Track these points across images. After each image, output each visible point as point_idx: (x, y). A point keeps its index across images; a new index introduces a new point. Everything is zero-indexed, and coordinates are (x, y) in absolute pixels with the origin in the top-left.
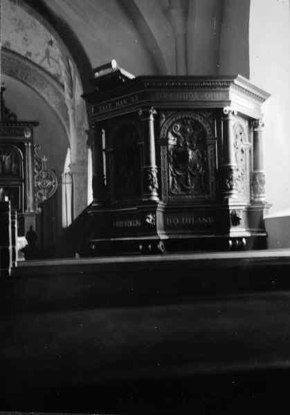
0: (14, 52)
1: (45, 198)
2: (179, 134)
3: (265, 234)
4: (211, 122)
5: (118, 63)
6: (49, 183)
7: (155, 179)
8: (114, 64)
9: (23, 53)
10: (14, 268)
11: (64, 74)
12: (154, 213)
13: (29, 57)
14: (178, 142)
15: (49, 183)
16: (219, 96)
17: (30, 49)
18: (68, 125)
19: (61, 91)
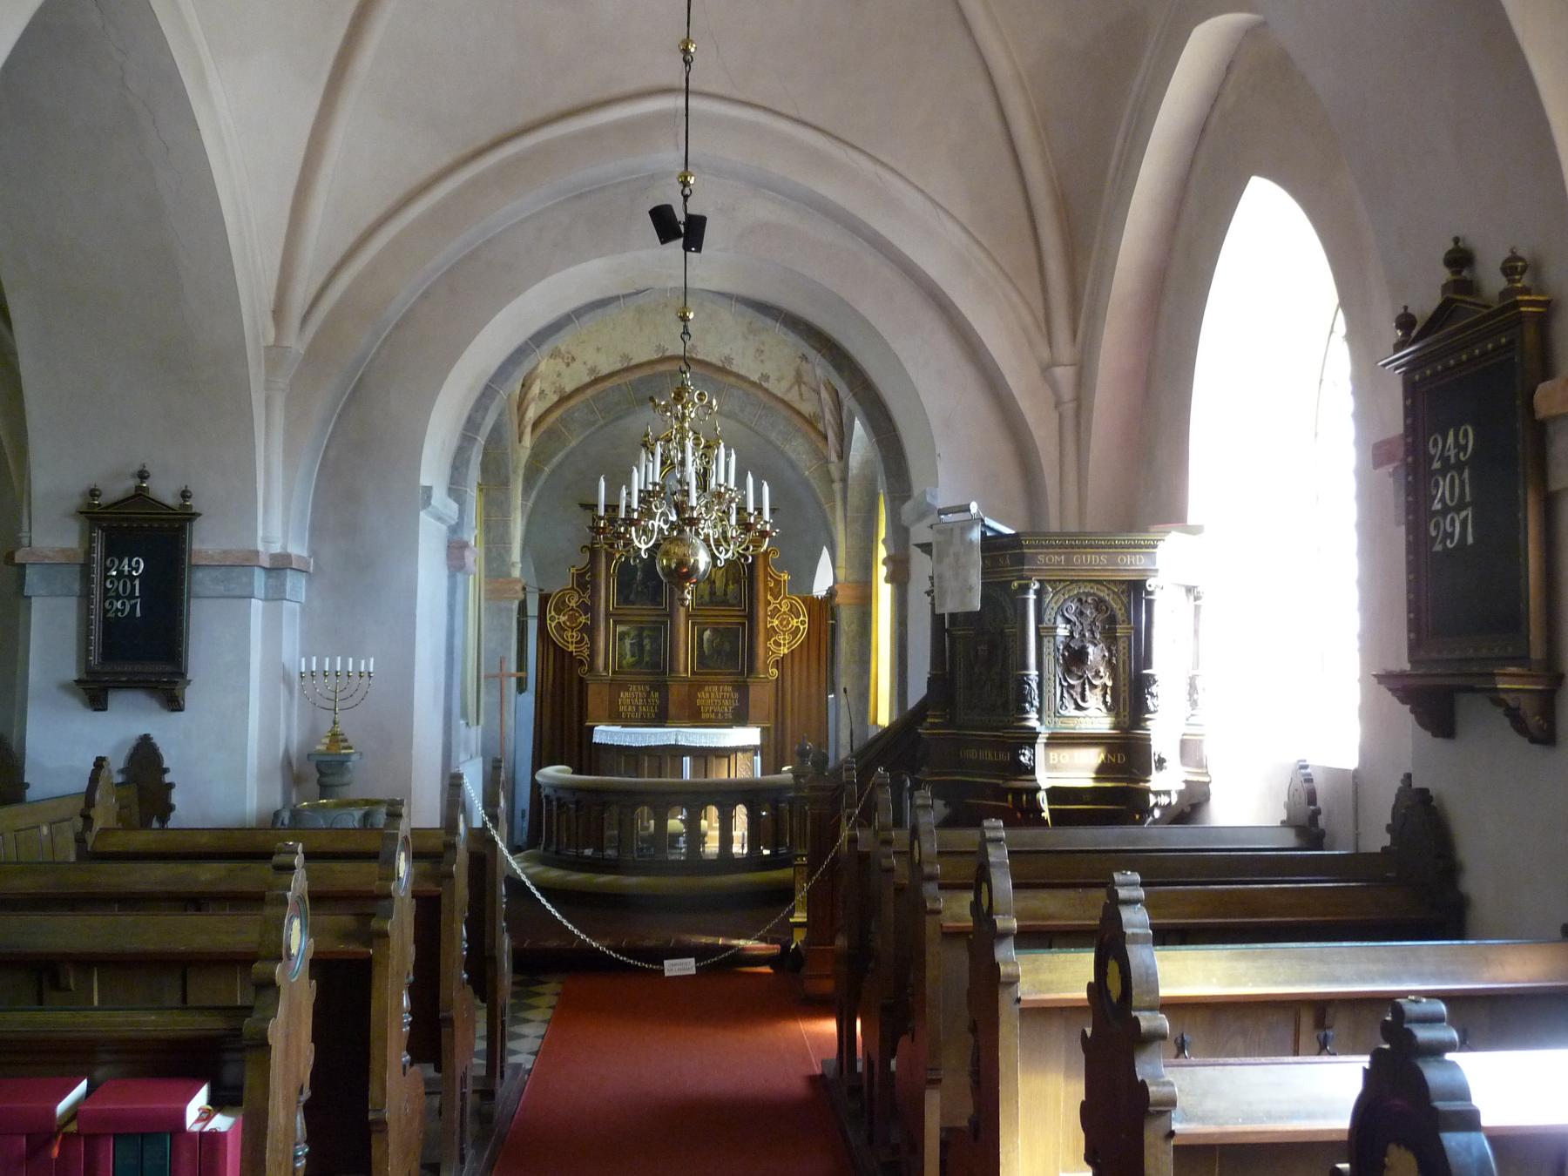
0: (737, 376)
1: (784, 650)
2: (1073, 618)
3: (1206, 779)
4: (1125, 600)
5: (980, 507)
6: (795, 622)
7: (1035, 692)
8: (974, 507)
9: (755, 378)
10: (470, 830)
11: (828, 416)
12: (1032, 746)
13: (765, 385)
14: (1071, 632)
15: (795, 622)
16: (1134, 563)
17: (769, 368)
18: (833, 508)
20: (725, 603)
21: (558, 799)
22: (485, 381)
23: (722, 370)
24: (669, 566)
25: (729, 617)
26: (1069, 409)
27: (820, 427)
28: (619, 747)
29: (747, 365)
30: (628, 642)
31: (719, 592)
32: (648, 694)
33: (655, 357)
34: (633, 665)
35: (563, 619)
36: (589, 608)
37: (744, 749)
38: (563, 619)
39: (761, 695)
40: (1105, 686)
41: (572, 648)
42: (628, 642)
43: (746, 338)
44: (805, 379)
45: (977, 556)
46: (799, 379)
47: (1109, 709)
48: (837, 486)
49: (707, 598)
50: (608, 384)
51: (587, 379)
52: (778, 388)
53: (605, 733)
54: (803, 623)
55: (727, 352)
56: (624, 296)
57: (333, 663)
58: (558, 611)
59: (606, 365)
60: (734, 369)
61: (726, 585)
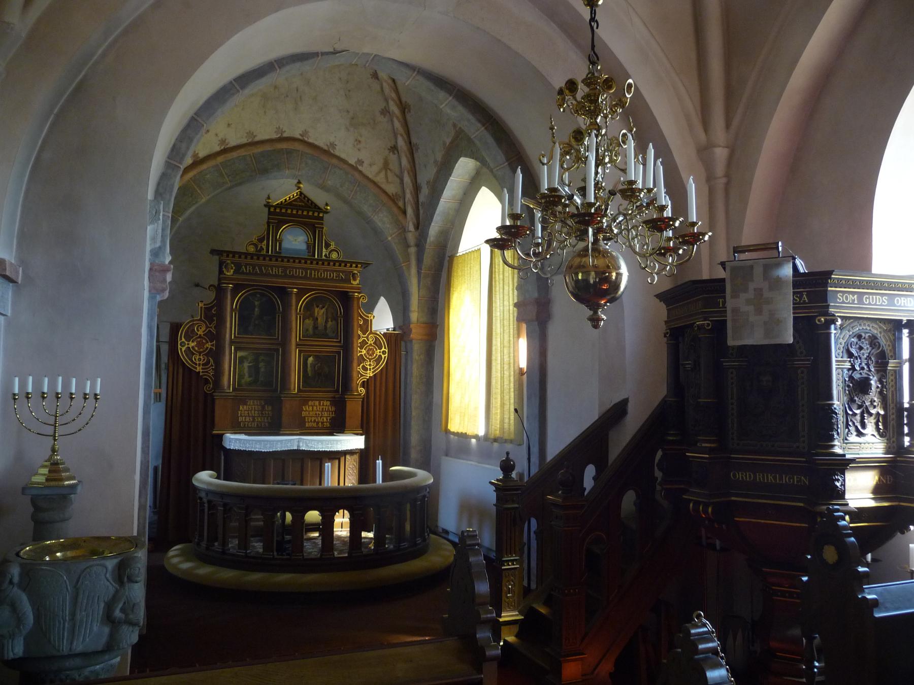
1: (370, 374)
9: (352, 161)
11: (408, 196)
13: (360, 168)
17: (363, 155)
18: (409, 267)
19: (401, 218)
20: (325, 335)
21: (209, 502)
22: (191, 113)
23: (326, 152)
24: (586, 281)
25: (329, 346)
26: (721, 182)
27: (401, 204)
28: (251, 453)
29: (346, 151)
30: (246, 365)
31: (321, 327)
32: (263, 407)
33: (275, 136)
34: (250, 384)
35: (192, 344)
36: (216, 336)
37: (351, 452)
38: (192, 344)
39: (354, 408)
40: (878, 414)
41: (199, 369)
42: (246, 365)
43: (348, 130)
44: (391, 166)
45: (789, 293)
46: (386, 166)
47: (881, 435)
48: (413, 250)
49: (311, 331)
50: (235, 154)
51: (218, 149)
52: (370, 171)
53: (235, 441)
54: (384, 353)
55: (332, 139)
56: (323, 54)
57: (53, 384)
58: (188, 338)
59: (234, 140)
60: (337, 153)
61: (326, 322)
